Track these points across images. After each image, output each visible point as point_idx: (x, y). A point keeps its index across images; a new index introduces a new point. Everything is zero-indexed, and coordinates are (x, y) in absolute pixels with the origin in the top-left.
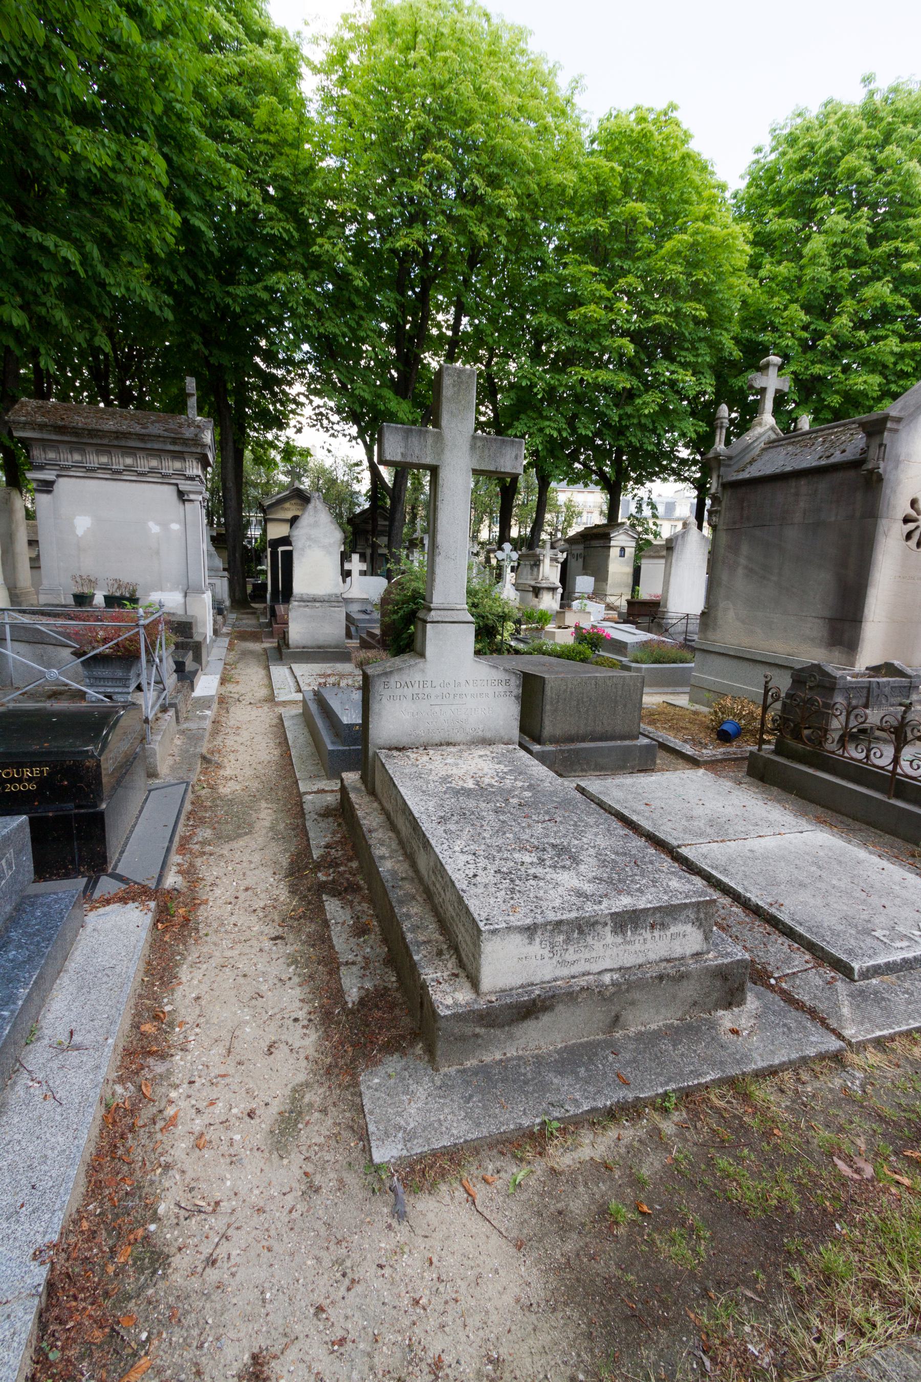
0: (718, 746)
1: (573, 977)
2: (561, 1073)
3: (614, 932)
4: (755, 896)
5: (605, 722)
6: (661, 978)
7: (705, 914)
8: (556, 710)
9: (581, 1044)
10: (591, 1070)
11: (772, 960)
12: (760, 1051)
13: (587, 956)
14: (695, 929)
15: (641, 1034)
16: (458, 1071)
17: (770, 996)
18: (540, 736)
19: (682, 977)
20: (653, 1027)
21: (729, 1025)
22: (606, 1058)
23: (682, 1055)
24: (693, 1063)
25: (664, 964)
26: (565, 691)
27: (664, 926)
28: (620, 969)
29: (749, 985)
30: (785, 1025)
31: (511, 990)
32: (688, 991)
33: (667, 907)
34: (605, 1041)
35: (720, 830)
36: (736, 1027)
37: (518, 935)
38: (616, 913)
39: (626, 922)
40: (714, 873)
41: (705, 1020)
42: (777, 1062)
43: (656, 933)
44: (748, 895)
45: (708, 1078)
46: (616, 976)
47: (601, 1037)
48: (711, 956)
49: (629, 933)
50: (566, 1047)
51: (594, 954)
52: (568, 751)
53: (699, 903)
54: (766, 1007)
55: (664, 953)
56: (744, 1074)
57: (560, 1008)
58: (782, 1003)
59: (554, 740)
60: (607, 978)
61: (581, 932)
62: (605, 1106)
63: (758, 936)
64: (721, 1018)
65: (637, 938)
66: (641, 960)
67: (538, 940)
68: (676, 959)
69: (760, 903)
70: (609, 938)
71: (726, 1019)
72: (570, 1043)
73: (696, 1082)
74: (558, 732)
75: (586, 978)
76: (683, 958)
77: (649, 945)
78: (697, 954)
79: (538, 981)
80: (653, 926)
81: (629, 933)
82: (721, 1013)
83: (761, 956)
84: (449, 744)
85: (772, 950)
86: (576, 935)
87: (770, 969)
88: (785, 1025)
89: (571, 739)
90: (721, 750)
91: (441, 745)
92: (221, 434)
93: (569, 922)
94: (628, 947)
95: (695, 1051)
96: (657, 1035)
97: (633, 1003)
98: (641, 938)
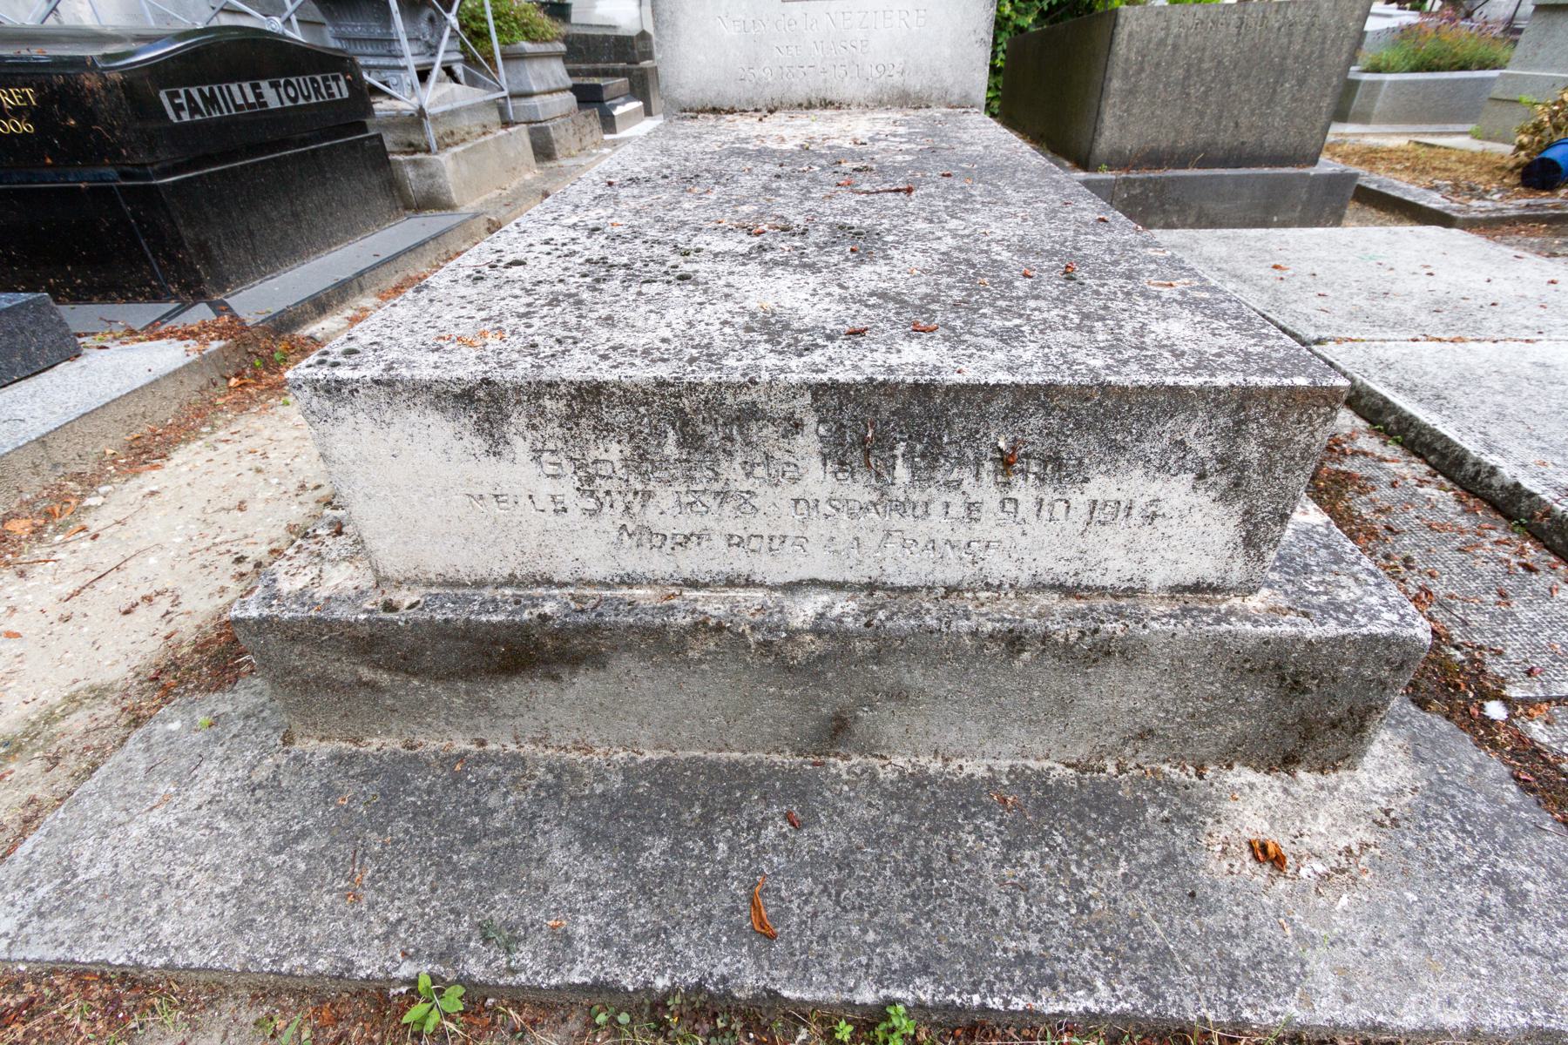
0: (1518, 195)
1: (694, 585)
2: (589, 838)
3: (838, 455)
4: (1513, 466)
5: (1243, 121)
6: (1014, 641)
7: (1271, 445)
8: (1132, 92)
9: (713, 766)
10: (685, 854)
11: (1514, 647)
12: (1347, 955)
13: (736, 527)
14: (1204, 499)
15: (920, 780)
16: (337, 757)
17: (1467, 753)
18: (1090, 151)
19: (1101, 652)
20: (975, 768)
21: (1255, 825)
22: (756, 827)
23: (1024, 886)
24: (1043, 929)
25: (1051, 600)
26: (1162, 42)
27: (1058, 468)
28: (871, 587)
29: (1397, 703)
30: (1497, 880)
31: (480, 584)
32: (1122, 695)
33: (1082, 393)
34: (790, 776)
35: (1456, 320)
36: (1279, 839)
37: (434, 417)
38: (834, 387)
39: (888, 427)
40: (1399, 400)
41: (1173, 787)
42: (1409, 1020)
43: (1024, 491)
44: (1491, 459)
45: (1079, 1003)
46: (844, 607)
47: (785, 759)
48: (1255, 603)
49: (902, 472)
50: (664, 762)
51: (759, 525)
52: (1143, 182)
53: (1247, 395)
54: (1437, 793)
55: (1051, 563)
56: (1240, 1026)
57: (624, 663)
58: (1511, 793)
59: (1119, 161)
60: (804, 610)
61: (691, 441)
62: (648, 988)
63: (1487, 570)
64: (1234, 793)
65: (939, 496)
66: (952, 575)
67: (521, 447)
68: (1102, 591)
69: (1527, 484)
70: (817, 479)
71: (1253, 801)
72: (682, 755)
73: (1019, 1003)
74: (1130, 144)
75: (740, 594)
76: (1131, 592)
77: (987, 527)
78: (1197, 588)
79: (565, 577)
80: (1006, 463)
81: (902, 472)
82: (1242, 776)
83: (1478, 624)
84: (827, 104)
85: (1524, 613)
86: (671, 449)
87: (1496, 668)
88: (1497, 880)
89: (1155, 159)
90: (1524, 202)
91: (810, 106)
92: (1068, 159)
93: (631, 397)
94: (895, 520)
95: (1078, 885)
96: (969, 797)
97: (899, 695)
98: (956, 499)
